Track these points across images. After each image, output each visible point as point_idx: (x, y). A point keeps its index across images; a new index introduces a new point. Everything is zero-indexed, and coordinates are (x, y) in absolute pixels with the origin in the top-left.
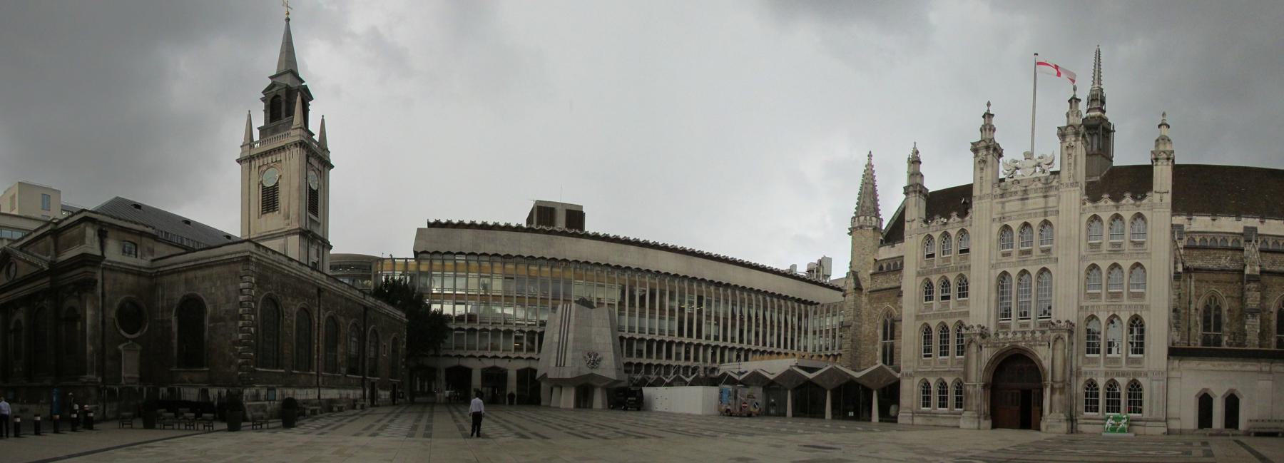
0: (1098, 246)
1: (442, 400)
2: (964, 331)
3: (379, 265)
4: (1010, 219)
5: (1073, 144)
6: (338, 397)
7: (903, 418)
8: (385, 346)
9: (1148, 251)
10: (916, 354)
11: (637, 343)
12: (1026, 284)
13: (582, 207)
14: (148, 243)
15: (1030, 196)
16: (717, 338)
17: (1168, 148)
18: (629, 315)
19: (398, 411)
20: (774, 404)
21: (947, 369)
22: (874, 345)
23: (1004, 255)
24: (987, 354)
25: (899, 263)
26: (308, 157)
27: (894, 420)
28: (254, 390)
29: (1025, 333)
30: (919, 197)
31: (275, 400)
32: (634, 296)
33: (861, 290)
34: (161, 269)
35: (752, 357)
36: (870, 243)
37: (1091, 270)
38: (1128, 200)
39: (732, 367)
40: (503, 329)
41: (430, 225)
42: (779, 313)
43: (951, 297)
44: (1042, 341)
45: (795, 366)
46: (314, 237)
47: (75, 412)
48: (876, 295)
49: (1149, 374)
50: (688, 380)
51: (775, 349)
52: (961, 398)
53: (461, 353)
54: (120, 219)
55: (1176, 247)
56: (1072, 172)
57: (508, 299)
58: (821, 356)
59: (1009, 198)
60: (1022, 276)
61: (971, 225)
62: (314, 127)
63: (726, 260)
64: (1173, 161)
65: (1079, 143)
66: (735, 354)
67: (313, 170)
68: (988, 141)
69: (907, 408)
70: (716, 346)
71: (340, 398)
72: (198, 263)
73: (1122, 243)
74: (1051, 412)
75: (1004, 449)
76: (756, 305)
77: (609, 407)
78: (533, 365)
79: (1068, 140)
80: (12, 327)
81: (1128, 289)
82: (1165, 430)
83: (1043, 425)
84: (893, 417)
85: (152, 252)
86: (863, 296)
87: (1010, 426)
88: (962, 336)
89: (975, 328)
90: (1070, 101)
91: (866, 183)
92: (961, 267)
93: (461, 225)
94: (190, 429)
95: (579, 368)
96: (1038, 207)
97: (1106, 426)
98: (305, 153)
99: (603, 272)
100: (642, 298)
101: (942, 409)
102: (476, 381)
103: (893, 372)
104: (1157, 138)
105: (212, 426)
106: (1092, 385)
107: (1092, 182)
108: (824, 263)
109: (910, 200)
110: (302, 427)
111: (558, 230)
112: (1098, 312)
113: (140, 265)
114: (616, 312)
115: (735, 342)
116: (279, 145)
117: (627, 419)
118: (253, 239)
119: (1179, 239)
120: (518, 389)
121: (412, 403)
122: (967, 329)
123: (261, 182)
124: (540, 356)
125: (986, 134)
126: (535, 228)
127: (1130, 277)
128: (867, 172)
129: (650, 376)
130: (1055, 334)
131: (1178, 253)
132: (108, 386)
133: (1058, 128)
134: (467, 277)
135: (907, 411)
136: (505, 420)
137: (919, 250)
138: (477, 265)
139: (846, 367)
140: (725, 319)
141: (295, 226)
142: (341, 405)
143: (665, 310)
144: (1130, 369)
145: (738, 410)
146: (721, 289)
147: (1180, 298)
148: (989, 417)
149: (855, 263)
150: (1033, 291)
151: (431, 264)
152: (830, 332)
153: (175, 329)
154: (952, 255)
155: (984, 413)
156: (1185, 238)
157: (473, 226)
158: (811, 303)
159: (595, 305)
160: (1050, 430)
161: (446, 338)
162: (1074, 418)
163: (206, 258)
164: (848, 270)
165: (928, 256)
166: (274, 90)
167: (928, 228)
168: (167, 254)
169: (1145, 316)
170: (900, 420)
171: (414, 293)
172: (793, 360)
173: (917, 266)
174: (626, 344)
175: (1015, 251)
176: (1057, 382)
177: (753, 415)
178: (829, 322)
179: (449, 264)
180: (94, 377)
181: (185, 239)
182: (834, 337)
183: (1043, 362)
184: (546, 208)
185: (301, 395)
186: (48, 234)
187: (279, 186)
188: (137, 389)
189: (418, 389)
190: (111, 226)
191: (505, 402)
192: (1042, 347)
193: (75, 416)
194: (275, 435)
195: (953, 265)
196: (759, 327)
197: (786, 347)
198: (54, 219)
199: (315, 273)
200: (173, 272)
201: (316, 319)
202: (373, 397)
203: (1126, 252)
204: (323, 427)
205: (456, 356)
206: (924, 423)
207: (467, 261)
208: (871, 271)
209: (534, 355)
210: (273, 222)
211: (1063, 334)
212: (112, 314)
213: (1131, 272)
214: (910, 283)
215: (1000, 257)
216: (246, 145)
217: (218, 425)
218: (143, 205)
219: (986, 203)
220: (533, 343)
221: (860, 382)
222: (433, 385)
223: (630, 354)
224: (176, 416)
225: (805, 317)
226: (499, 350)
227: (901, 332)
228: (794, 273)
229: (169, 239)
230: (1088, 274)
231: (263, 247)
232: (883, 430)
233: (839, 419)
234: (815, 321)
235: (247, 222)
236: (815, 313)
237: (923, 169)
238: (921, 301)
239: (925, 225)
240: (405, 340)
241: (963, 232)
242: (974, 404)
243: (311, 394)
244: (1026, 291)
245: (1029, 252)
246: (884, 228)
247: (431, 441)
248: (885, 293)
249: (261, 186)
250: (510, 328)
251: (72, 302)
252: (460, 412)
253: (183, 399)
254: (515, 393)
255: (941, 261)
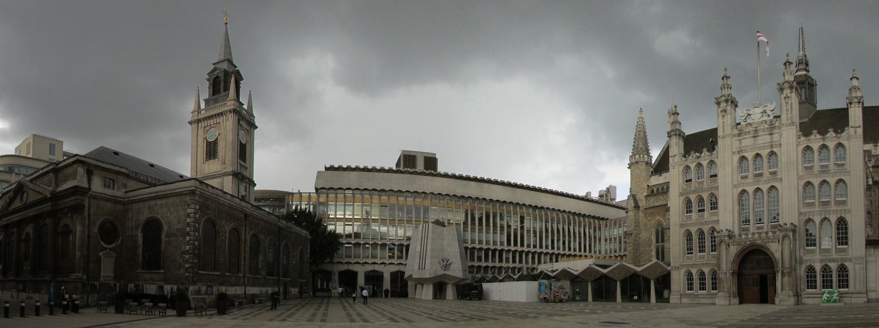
0: (811, 168)
1: (336, 295)
2: (716, 234)
3: (290, 198)
4: (746, 151)
5: (789, 95)
6: (259, 292)
7: (674, 299)
8: (294, 256)
9: (848, 170)
10: (682, 252)
11: (477, 251)
12: (759, 198)
13: (435, 154)
14: (122, 179)
15: (760, 134)
16: (535, 246)
17: (859, 94)
18: (471, 231)
19: (303, 303)
20: (578, 293)
21: (705, 262)
22: (649, 247)
23: (742, 178)
24: (734, 250)
25: (665, 187)
26: (239, 120)
27: (667, 301)
28: (197, 287)
29: (761, 234)
30: (679, 138)
31: (212, 294)
32: (475, 218)
33: (639, 208)
34: (131, 199)
35: (561, 259)
36: (644, 174)
37: (807, 186)
38: (831, 134)
39: (547, 266)
40: (380, 243)
41: (327, 169)
42: (580, 226)
43: (705, 210)
44: (774, 239)
45: (593, 264)
46: (244, 177)
47: (66, 300)
48: (649, 211)
49: (853, 260)
50: (515, 277)
51: (577, 253)
52: (716, 283)
53: (350, 260)
54: (103, 162)
55: (867, 167)
56: (789, 115)
57: (383, 222)
58: (611, 257)
59: (745, 137)
60: (757, 192)
61: (717, 157)
62: (243, 99)
63: (540, 190)
64: (863, 104)
65: (794, 94)
66: (548, 257)
67: (243, 130)
68: (727, 96)
69: (676, 291)
70: (535, 252)
71: (261, 294)
72: (158, 194)
73: (829, 165)
74: (782, 290)
75: (752, 319)
76: (563, 222)
77: (458, 298)
78: (402, 268)
79: (785, 92)
80: (23, 237)
81: (835, 199)
82: (866, 299)
83: (777, 300)
84: (666, 299)
85: (125, 186)
86: (641, 212)
87: (752, 301)
88: (715, 237)
89: (724, 231)
90: (785, 64)
91: (639, 131)
92: (712, 188)
93: (349, 169)
94: (149, 315)
95: (436, 271)
96: (766, 142)
97: (823, 299)
98: (237, 118)
99: (452, 201)
100: (480, 219)
101: (702, 291)
102: (361, 280)
103: (665, 266)
104: (850, 88)
105: (166, 313)
106: (811, 270)
107: (802, 122)
108: (611, 191)
109: (672, 141)
110: (232, 314)
111: (418, 171)
112: (813, 216)
113: (116, 195)
114: (462, 229)
115: (548, 249)
116: (221, 111)
117: (471, 306)
118: (200, 178)
119: (868, 161)
120: (391, 286)
121: (314, 295)
122: (718, 232)
123: (206, 138)
124: (407, 262)
125: (725, 91)
126: (402, 170)
127: (836, 189)
128: (639, 123)
129: (488, 275)
130: (783, 233)
131: (868, 171)
132: (91, 282)
133: (777, 84)
134: (353, 205)
135: (676, 294)
136: (381, 309)
137: (681, 176)
138: (361, 197)
139: (630, 264)
140: (541, 232)
141: (229, 169)
142: (260, 299)
143: (497, 227)
144: (839, 257)
145: (552, 298)
146: (537, 211)
147: (871, 203)
148: (737, 295)
149: (634, 189)
150: (765, 203)
151: (327, 196)
152: (617, 239)
153: (140, 241)
154: (705, 180)
155: (733, 294)
156: (873, 160)
157: (357, 169)
158: (603, 219)
159: (446, 224)
160: (781, 304)
161: (339, 250)
162: (799, 294)
163: (164, 191)
164: (629, 194)
165: (687, 181)
166: (215, 73)
167: (686, 160)
168: (136, 187)
169: (848, 217)
170: (671, 300)
171: (316, 218)
172: (591, 260)
173: (679, 188)
174: (469, 252)
175: (751, 174)
176: (785, 268)
177: (564, 301)
178: (616, 232)
179: (340, 196)
180: (81, 275)
181: (149, 178)
182: (620, 243)
183: (775, 254)
184: (409, 156)
185: (231, 291)
186: (51, 172)
187: (218, 141)
188: (112, 285)
189: (319, 287)
190: (96, 166)
191: (382, 296)
192: (774, 244)
193: (66, 303)
194: (211, 319)
195: (705, 186)
196: (565, 237)
197: (585, 251)
198: (57, 161)
199: (243, 203)
200: (140, 201)
201: (243, 236)
202: (286, 292)
203: (831, 171)
204: (247, 314)
205: (346, 263)
206: (690, 302)
207: (353, 194)
208: (645, 194)
209: (402, 261)
210: (213, 167)
211: (789, 233)
212: (95, 230)
213: (836, 186)
214: (675, 201)
215: (740, 180)
216: (196, 111)
217: (170, 312)
218: (120, 152)
219: (728, 141)
220: (402, 252)
221: (640, 274)
222: (330, 284)
223: (472, 259)
224: (139, 305)
225: (599, 230)
226: (377, 258)
227: (669, 237)
228: (589, 197)
229: (138, 177)
230: (805, 189)
231: (205, 183)
232: (660, 308)
233: (627, 301)
234: (606, 232)
235: (195, 167)
236: (606, 226)
237: (680, 118)
238: (683, 213)
239: (683, 159)
240: (309, 251)
241: (712, 162)
242: (726, 287)
243: (238, 290)
244: (760, 203)
245: (761, 175)
246: (653, 163)
247: (325, 325)
248: (653, 210)
249: (205, 141)
250: (385, 242)
251: (67, 221)
252: (349, 304)
253: (145, 292)
254: (389, 289)
255: (697, 184)
